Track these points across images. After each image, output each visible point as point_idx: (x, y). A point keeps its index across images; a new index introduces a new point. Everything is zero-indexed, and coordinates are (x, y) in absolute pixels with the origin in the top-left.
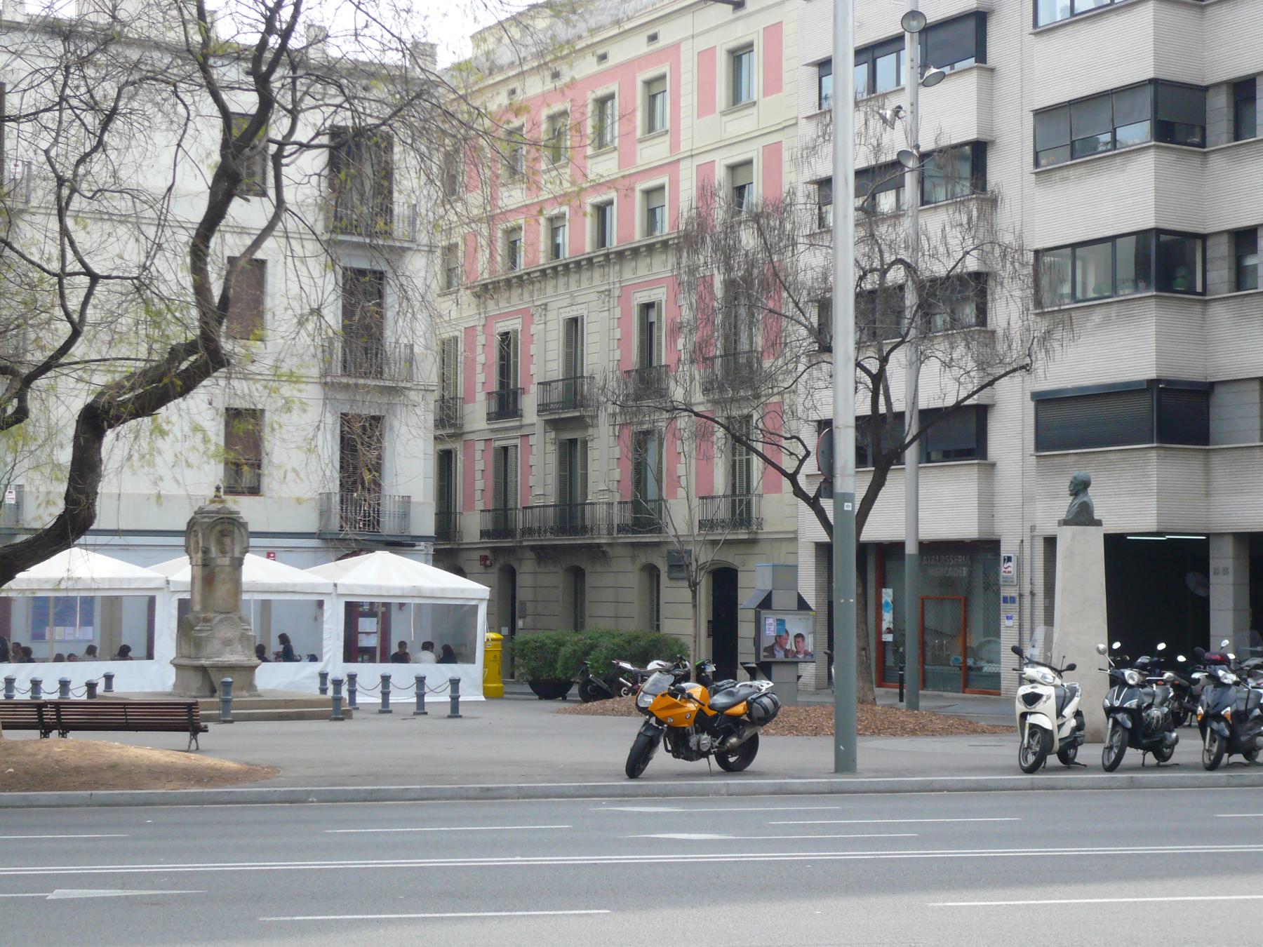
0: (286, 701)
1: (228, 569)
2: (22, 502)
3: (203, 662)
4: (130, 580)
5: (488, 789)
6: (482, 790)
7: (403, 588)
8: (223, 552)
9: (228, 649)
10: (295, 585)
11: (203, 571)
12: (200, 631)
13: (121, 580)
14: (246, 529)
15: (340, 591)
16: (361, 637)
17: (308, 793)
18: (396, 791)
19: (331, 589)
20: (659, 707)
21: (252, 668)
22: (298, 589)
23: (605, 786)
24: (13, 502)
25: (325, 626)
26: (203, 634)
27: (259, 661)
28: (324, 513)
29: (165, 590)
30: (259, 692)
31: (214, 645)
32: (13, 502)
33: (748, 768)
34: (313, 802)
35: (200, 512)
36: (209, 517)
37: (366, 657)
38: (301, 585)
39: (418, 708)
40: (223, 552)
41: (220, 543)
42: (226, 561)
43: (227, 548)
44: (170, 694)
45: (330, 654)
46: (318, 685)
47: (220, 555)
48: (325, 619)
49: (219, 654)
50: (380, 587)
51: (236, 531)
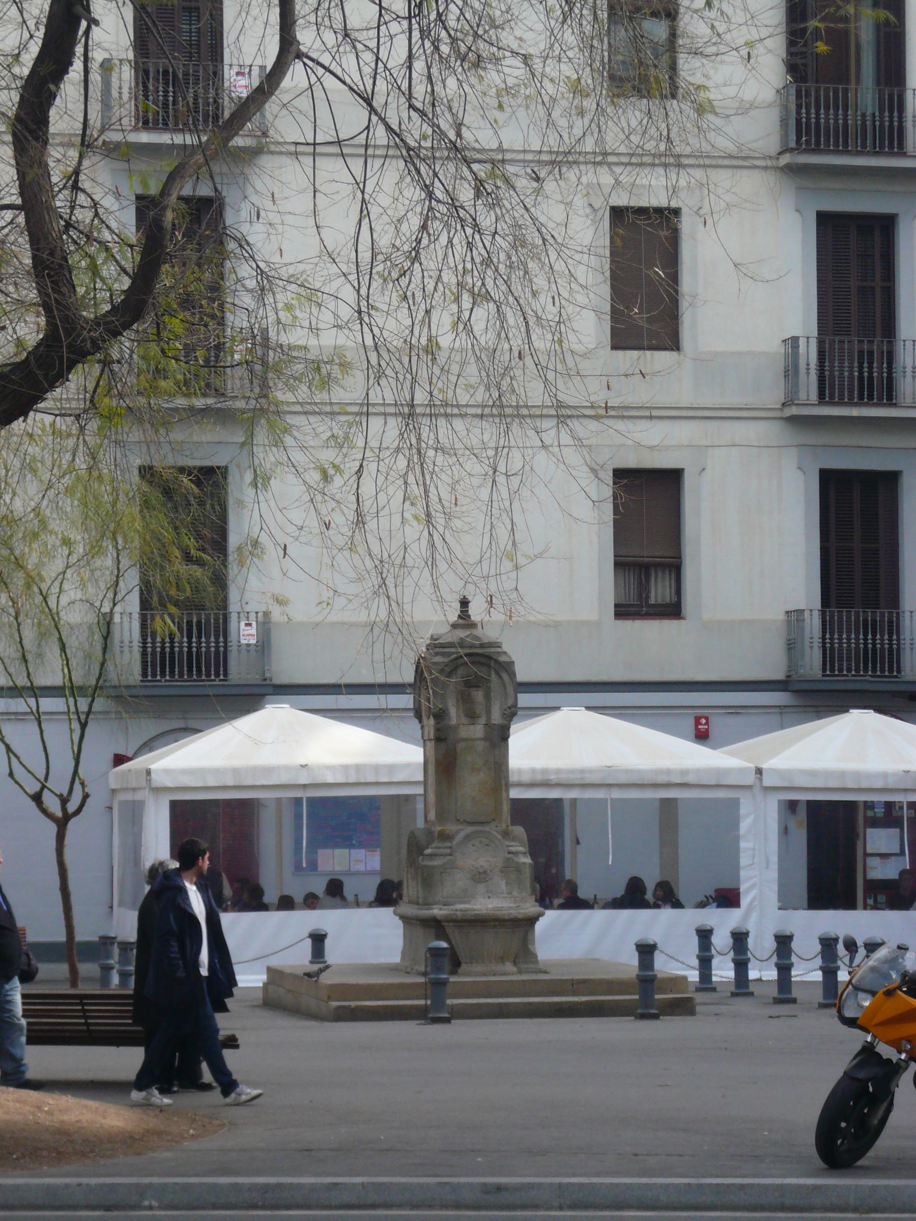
0: (573, 982)
1: (481, 746)
2: (269, 643)
3: (437, 911)
4: (391, 768)
5: (499, 1188)
6: (487, 1189)
7: (885, 775)
8: (472, 716)
9: (481, 888)
10: (684, 772)
11: (436, 749)
12: (432, 856)
13: (377, 768)
14: (512, 675)
15: (767, 781)
16: (872, 862)
17: (142, 1190)
18: (313, 1188)
19: (750, 779)
20: (879, 1018)
21: (532, 921)
22: (691, 779)
23: (742, 1187)
24: (253, 641)
25: (743, 845)
26: (437, 862)
27: (542, 909)
28: (792, 646)
29: (757, 790)
30: (541, 966)
31: (458, 881)
32: (253, 641)
33: (860, 1163)
34: (151, 1208)
35: (436, 646)
36: (443, 654)
37: (882, 898)
38: (698, 771)
39: (826, 996)
40: (472, 716)
41: (465, 700)
42: (478, 731)
43: (480, 709)
44: (393, 969)
45: (754, 893)
46: (696, 951)
47: (465, 720)
48: (742, 831)
49: (465, 896)
50: (843, 774)
51: (494, 677)
